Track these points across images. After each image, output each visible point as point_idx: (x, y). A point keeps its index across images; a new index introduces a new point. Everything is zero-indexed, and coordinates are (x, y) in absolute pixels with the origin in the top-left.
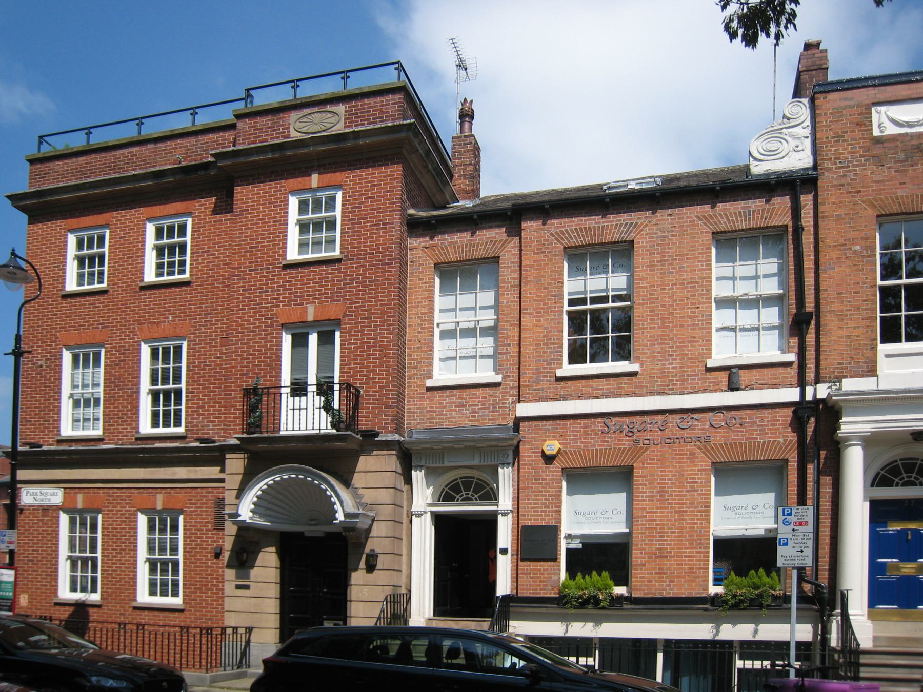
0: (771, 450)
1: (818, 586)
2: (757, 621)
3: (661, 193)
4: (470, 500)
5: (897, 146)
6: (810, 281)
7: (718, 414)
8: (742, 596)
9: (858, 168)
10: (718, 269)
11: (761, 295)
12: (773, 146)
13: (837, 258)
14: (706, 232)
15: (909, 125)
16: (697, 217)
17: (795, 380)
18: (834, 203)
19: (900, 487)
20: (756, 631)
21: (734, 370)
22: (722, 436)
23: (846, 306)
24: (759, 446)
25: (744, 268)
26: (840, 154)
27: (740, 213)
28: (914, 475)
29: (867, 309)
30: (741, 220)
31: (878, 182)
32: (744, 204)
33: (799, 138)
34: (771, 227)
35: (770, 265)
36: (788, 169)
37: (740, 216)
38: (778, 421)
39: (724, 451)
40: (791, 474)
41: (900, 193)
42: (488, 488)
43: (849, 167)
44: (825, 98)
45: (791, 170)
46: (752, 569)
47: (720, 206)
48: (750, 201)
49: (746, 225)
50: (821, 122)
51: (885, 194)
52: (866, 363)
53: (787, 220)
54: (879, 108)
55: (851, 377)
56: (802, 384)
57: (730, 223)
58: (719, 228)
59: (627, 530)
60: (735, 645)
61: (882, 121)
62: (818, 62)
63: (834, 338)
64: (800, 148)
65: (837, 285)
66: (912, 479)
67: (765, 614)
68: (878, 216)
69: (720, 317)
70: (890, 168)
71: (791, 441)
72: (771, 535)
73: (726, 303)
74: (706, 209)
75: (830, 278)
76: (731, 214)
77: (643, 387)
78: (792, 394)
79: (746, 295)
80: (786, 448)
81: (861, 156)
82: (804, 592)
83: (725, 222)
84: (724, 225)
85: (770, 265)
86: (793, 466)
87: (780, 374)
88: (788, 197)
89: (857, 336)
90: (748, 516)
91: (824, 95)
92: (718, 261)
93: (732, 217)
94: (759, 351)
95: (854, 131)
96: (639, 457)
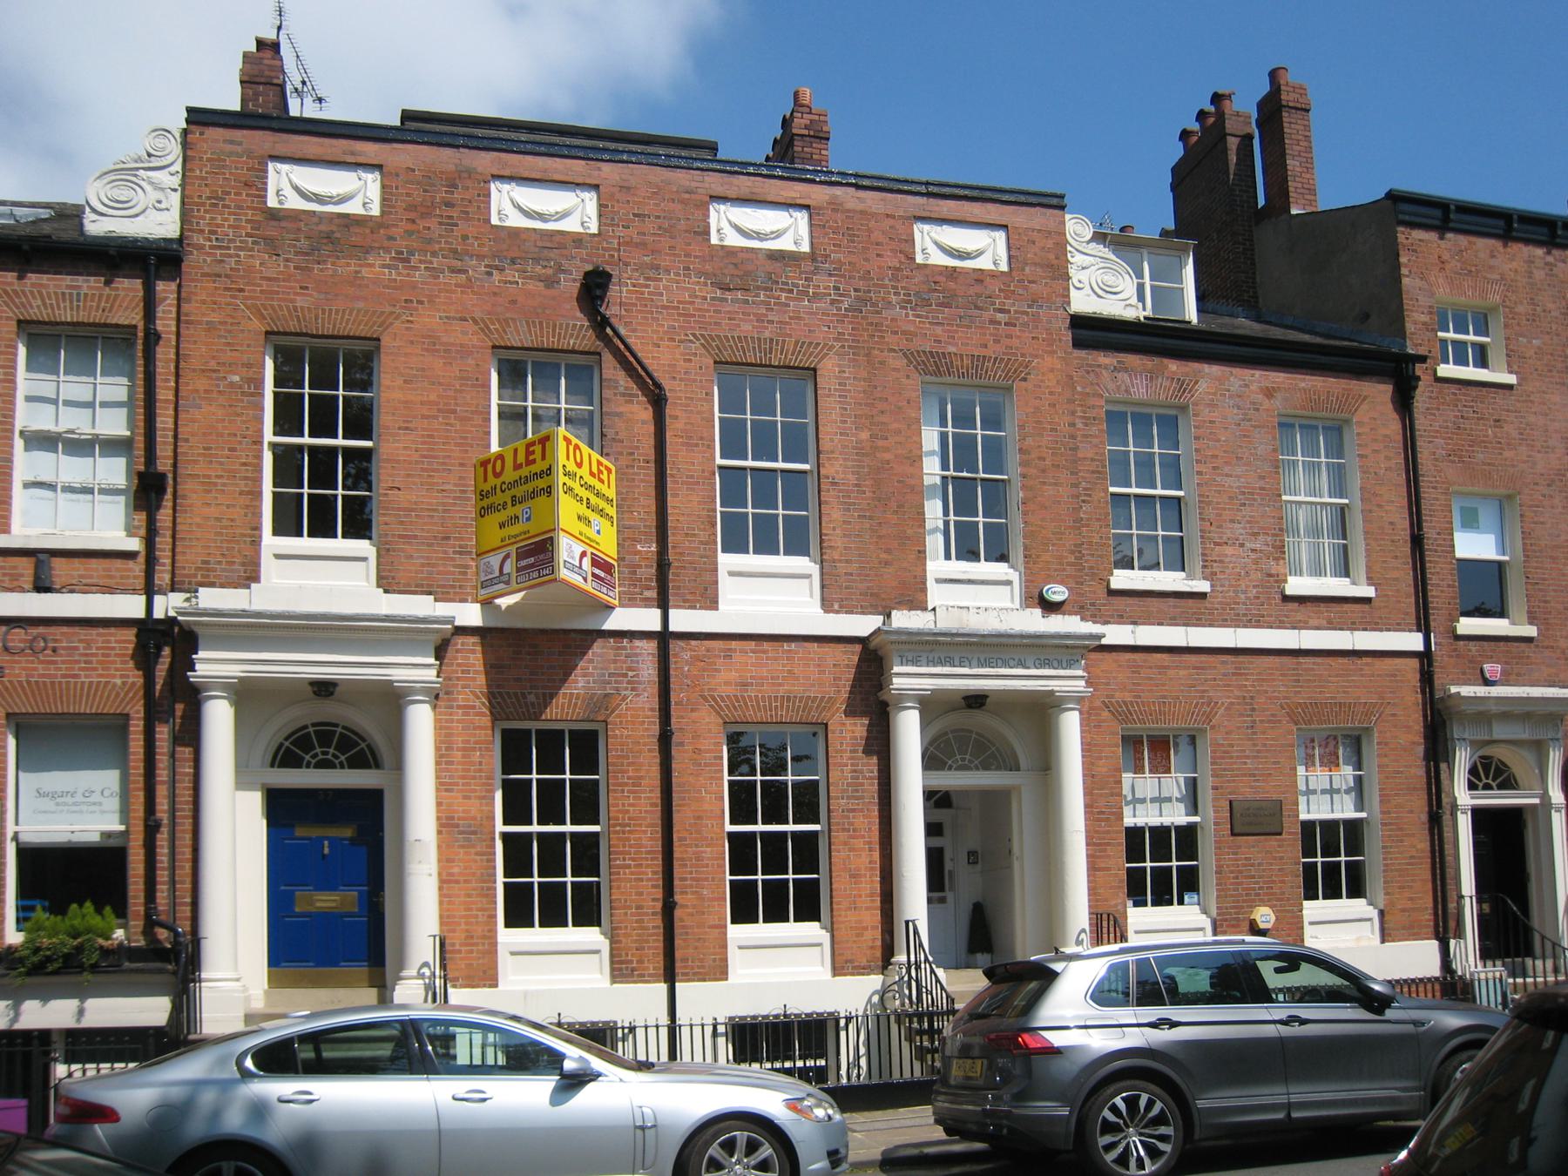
0: (101, 696)
1: (177, 934)
2: (82, 993)
4: (1490, 788)
5: (299, 230)
6: (166, 423)
7: (17, 630)
8: (49, 949)
9: (242, 253)
10: (25, 382)
11: (97, 435)
12: (123, 194)
14: (8, 318)
15: (318, 199)
17: (140, 583)
18: (204, 302)
20: (81, 1012)
21: (42, 557)
22: (24, 669)
23: (216, 470)
24: (82, 689)
25: (75, 387)
26: (218, 226)
27: (63, 294)
28: (331, 751)
29: (246, 478)
30: (65, 307)
31: (269, 279)
32: (72, 280)
33: (162, 189)
34: (111, 325)
35: (115, 388)
36: (141, 235)
37: (64, 301)
38: (113, 648)
39: (26, 694)
40: (135, 740)
41: (300, 302)
43: (228, 248)
44: (202, 134)
45: (146, 239)
46: (74, 902)
47: (32, 278)
48: (80, 278)
49: (72, 316)
50: (193, 170)
51: (279, 300)
52: (243, 564)
53: (136, 318)
54: (279, 166)
55: (222, 586)
56: (150, 591)
57: (46, 308)
58: (30, 316)
59: (122, 828)
60: (55, 1038)
61: (282, 186)
62: (267, 73)
63: (198, 520)
64: (163, 206)
65: (204, 434)
66: (329, 757)
67: (88, 981)
68: (267, 333)
69: (25, 464)
70: (287, 260)
71: (134, 684)
72: (113, 843)
73: (42, 441)
74: (9, 280)
75: (193, 421)
76: (48, 294)
78: (131, 606)
79: (72, 432)
80: (127, 694)
81: (248, 235)
82: (159, 941)
83: (38, 307)
84: (37, 311)
85: (115, 388)
86: (137, 726)
87: (118, 570)
88: (139, 281)
89: (232, 520)
90: (75, 808)
91: (201, 129)
92: (30, 368)
93: (50, 299)
94: (93, 529)
95: (240, 194)
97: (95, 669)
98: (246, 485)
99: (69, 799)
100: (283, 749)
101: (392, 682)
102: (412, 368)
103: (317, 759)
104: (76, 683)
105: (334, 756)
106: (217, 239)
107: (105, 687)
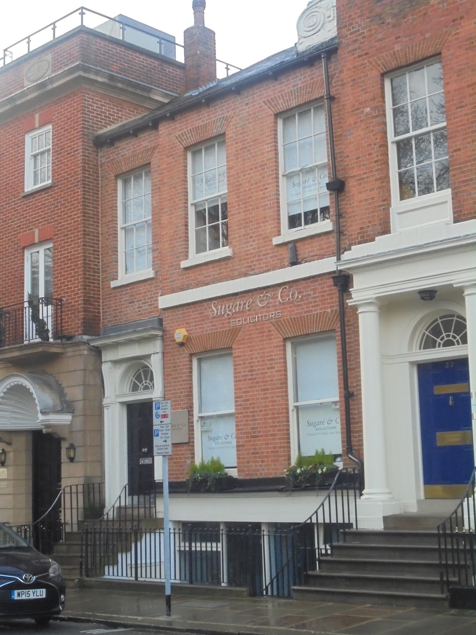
3: (206, 99)
13: (355, 123)
14: (271, 115)
16: (264, 102)
19: (441, 348)
41: (397, 47)
42: (455, 319)
52: (380, 224)
63: (356, 204)
71: (336, 310)
77: (234, 270)
96: (235, 339)
97: (318, 305)
98: (378, 174)
99: (321, 426)
100: (426, 336)
101: (451, 285)
102: (461, 65)
103: (444, 341)
104: (311, 315)
105: (442, 339)
106: (353, 27)
107: (324, 315)
